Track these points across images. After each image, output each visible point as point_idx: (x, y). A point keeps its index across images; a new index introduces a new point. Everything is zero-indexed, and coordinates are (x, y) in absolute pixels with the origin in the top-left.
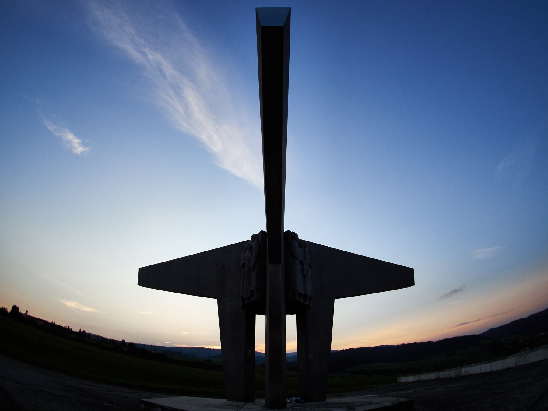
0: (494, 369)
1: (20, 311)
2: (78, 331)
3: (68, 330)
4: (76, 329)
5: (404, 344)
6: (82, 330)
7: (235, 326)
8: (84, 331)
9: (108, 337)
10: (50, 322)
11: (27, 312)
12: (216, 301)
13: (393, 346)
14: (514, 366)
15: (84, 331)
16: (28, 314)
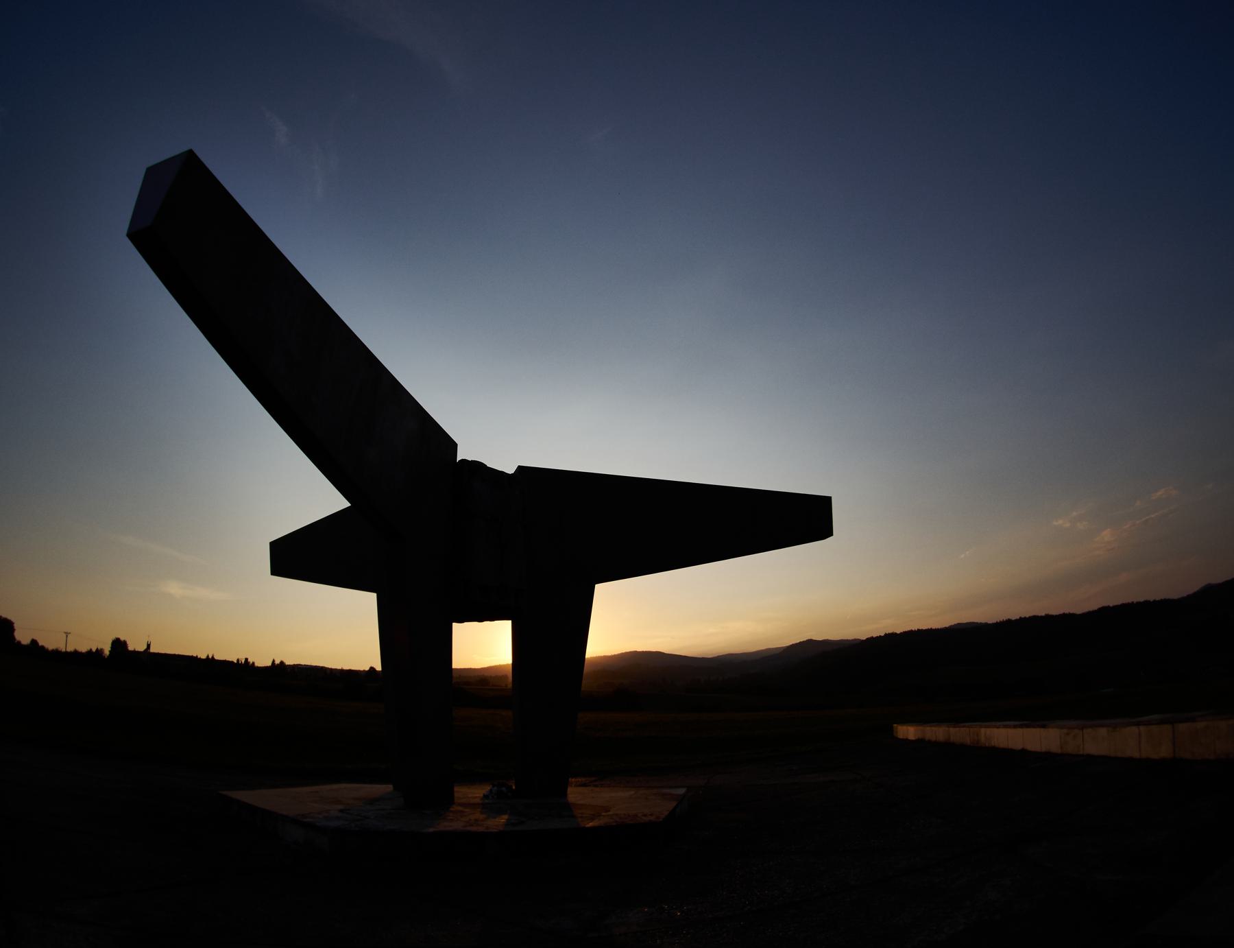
0: (1030, 747)
1: (131, 648)
2: (269, 664)
3: (246, 668)
4: (263, 661)
5: (1009, 621)
6: (277, 662)
7: (414, 636)
8: (282, 663)
9: (1196, 589)
10: (204, 657)
11: (149, 646)
12: (374, 596)
13: (986, 625)
14: (1059, 751)
15: (282, 663)
16: (152, 650)
